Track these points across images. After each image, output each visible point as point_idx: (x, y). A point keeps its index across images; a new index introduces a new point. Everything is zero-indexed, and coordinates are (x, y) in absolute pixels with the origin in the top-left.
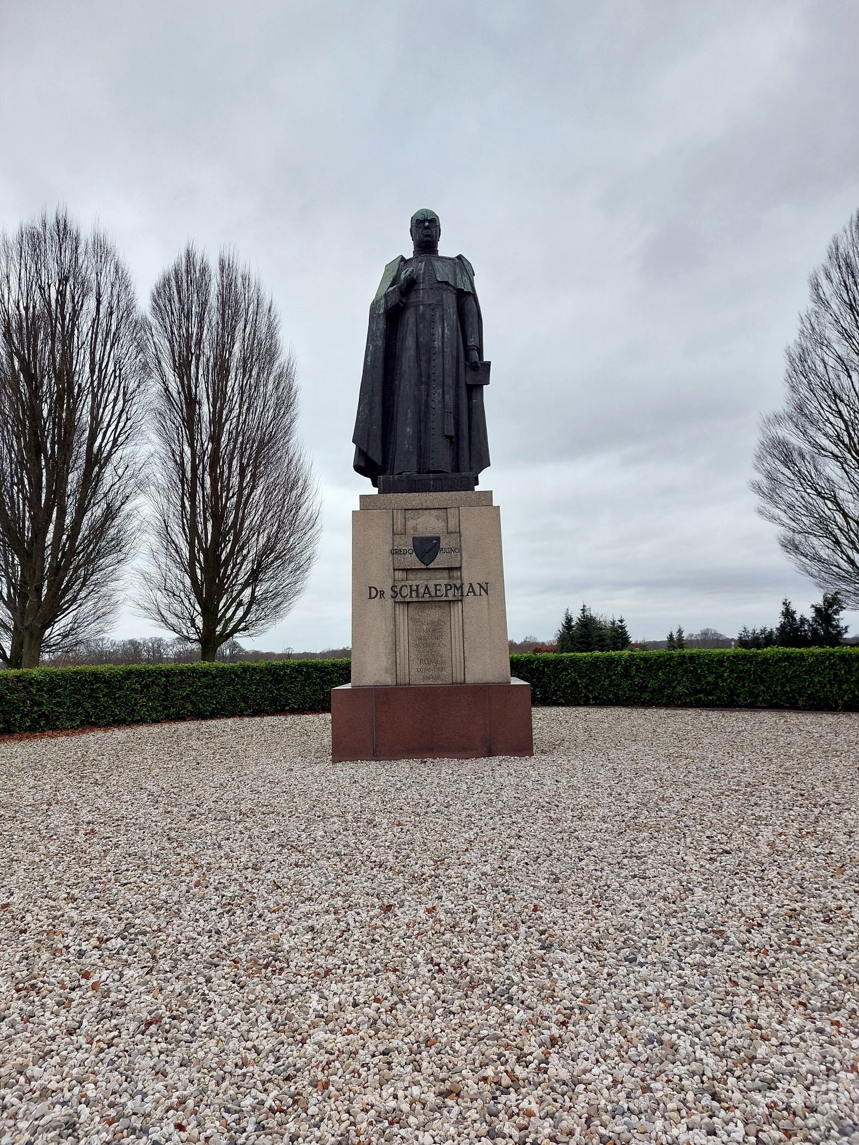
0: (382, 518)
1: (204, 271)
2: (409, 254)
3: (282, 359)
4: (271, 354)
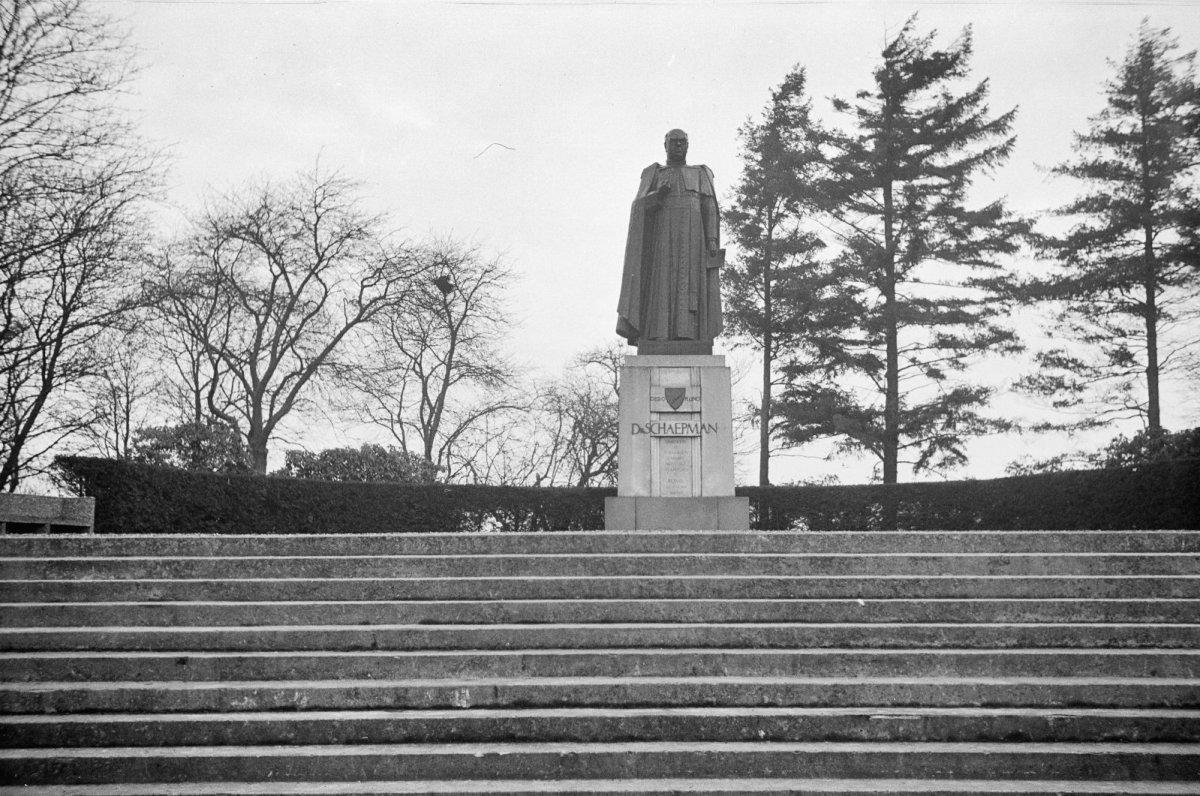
2: (663, 162)
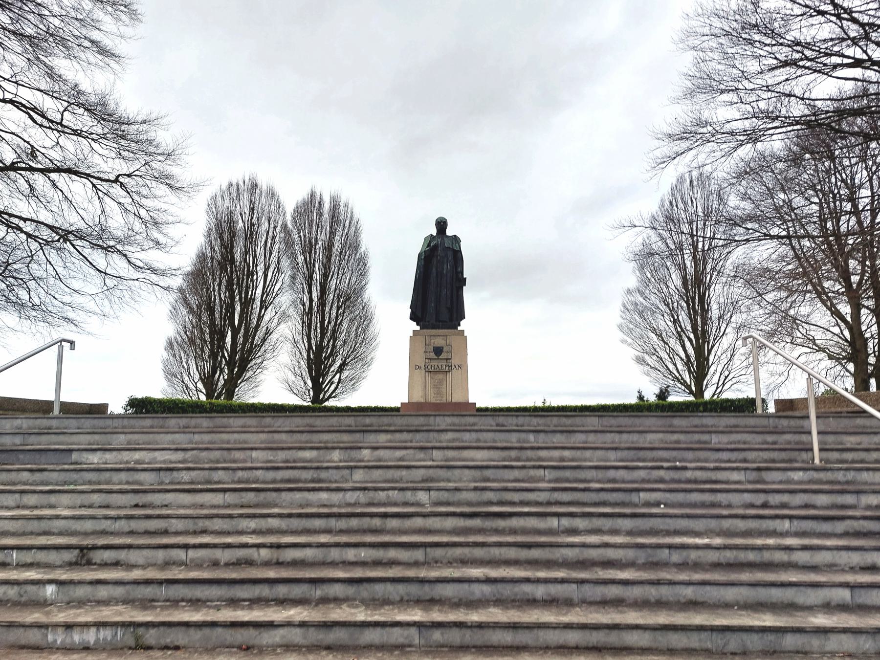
0: (421, 339)
1: (321, 200)
2: (435, 234)
3: (362, 250)
4: (356, 246)
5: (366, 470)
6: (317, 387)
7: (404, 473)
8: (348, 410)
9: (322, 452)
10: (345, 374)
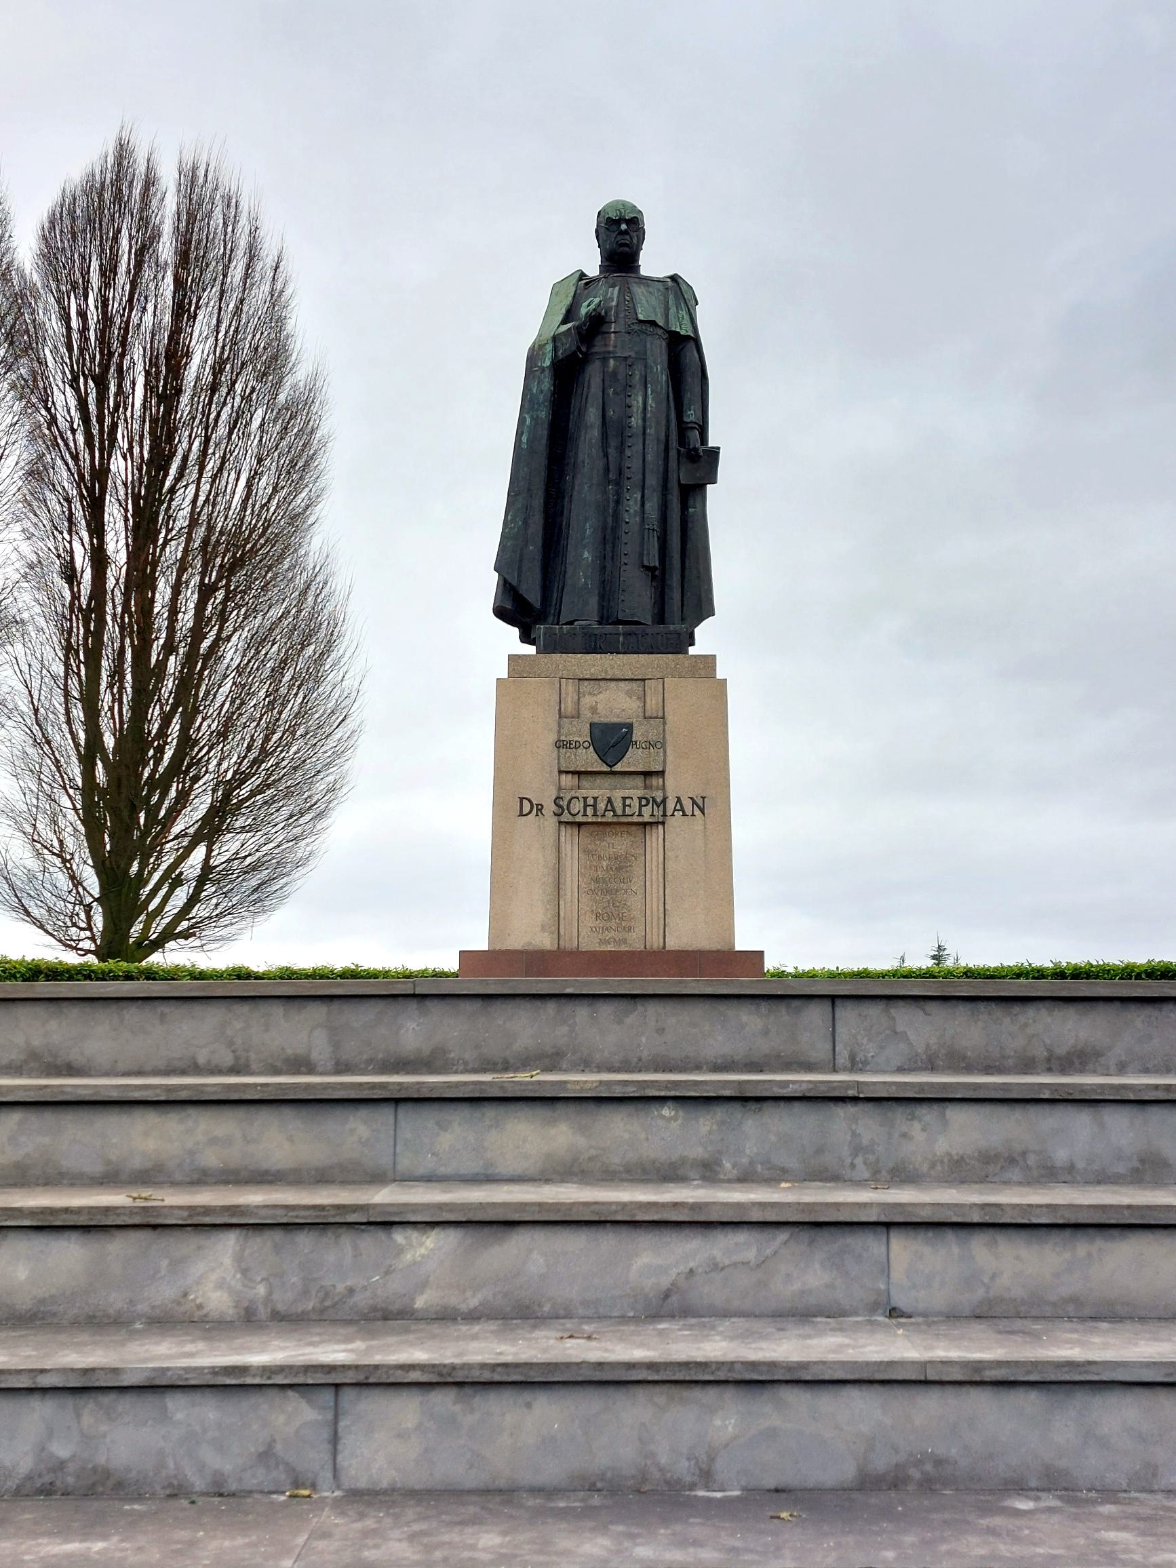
0: (541, 693)
1: (149, 183)
2: (593, 271)
3: (298, 376)
4: (273, 361)
5: (444, 1401)
6: (121, 897)
7: (726, 1420)
8: (244, 990)
9: (117, 1247)
10: (228, 846)
